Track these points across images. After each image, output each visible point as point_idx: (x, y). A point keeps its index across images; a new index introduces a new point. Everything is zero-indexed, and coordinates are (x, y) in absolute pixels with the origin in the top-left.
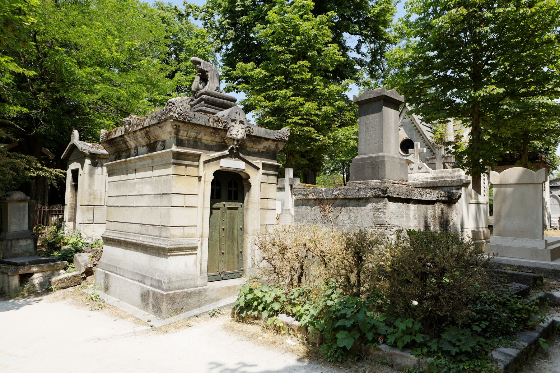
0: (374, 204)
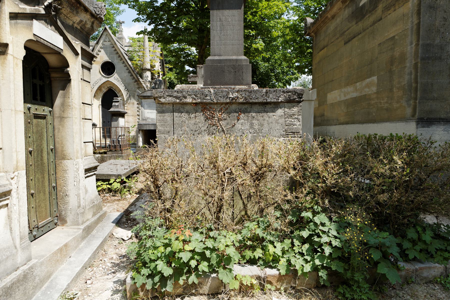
0: (286, 110)
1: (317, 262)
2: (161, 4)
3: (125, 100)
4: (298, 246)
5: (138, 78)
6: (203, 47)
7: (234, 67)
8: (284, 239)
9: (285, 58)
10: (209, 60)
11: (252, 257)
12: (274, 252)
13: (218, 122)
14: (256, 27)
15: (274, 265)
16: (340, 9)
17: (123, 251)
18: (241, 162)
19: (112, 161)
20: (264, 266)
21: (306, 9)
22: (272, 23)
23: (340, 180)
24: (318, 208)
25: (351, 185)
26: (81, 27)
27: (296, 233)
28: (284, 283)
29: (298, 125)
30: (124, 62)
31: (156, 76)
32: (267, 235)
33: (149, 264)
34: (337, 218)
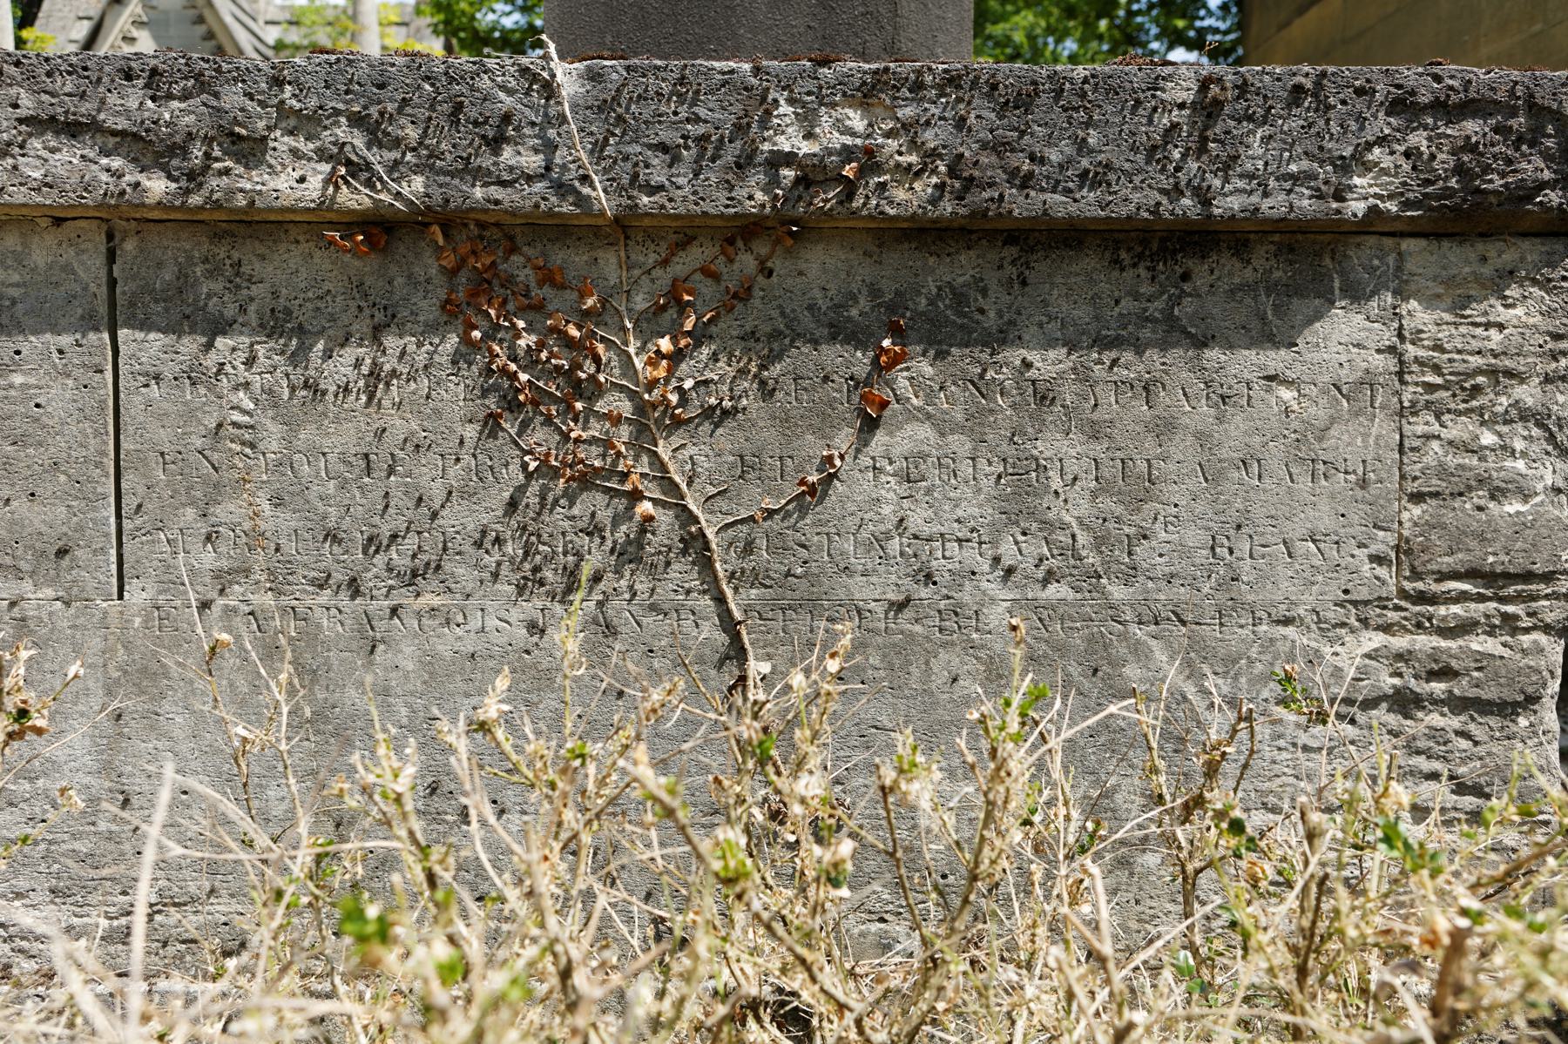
0: (1418, 315)
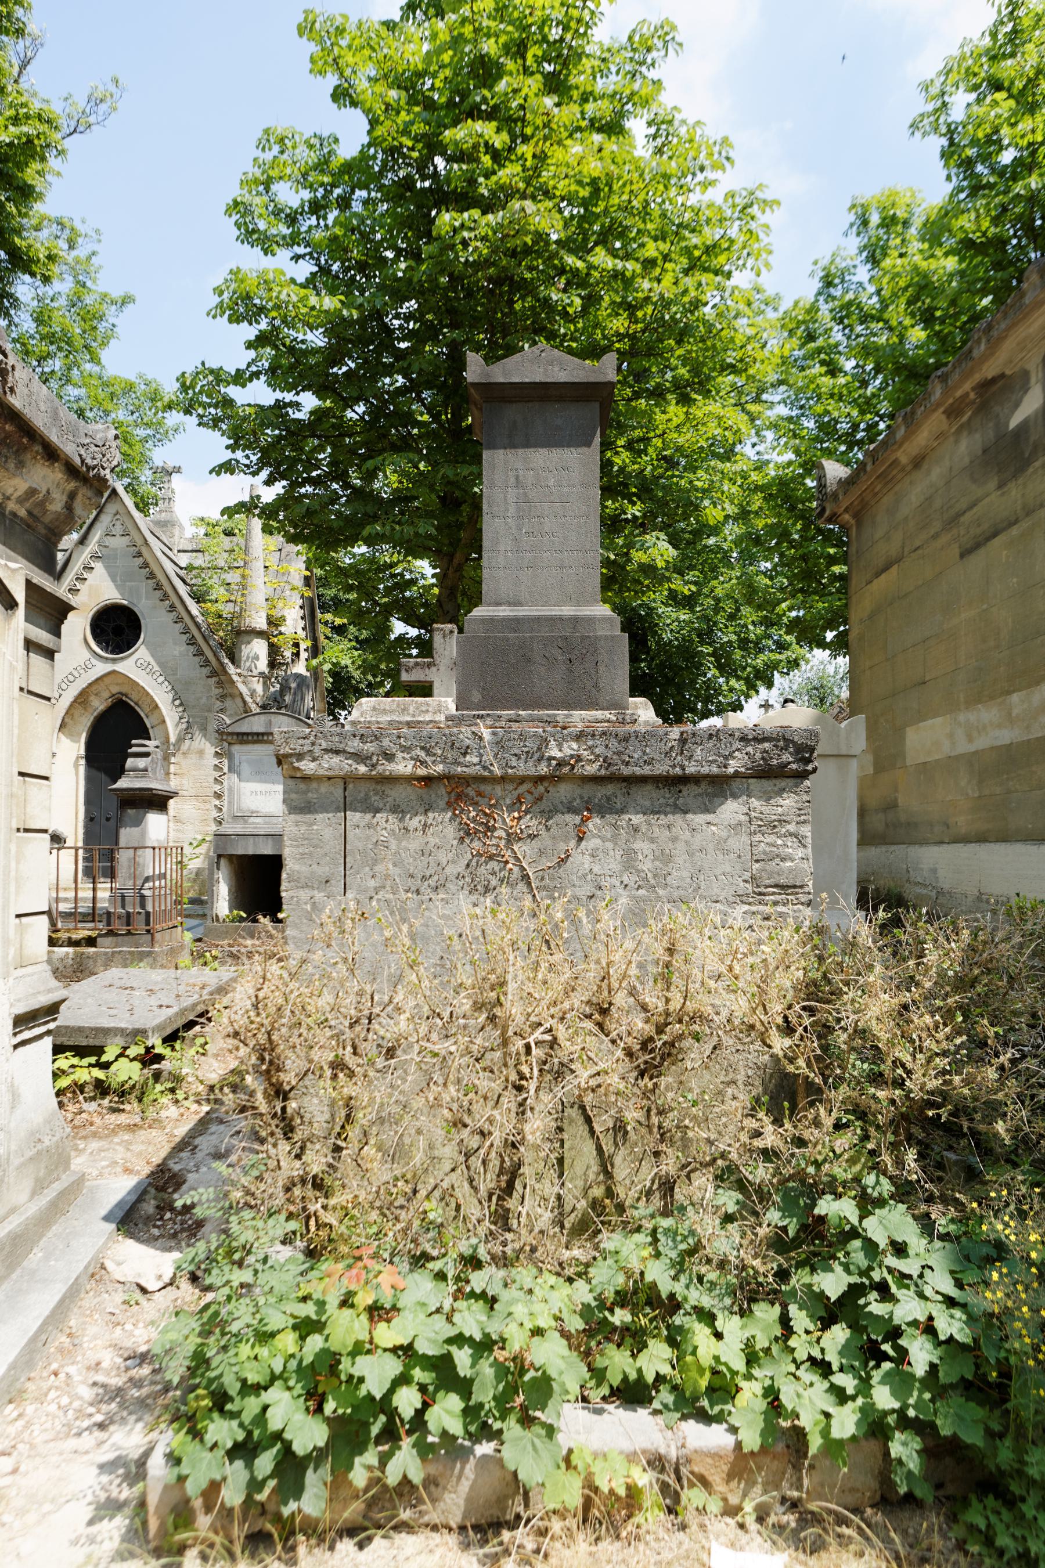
0: (755, 803)
1: (884, 1398)
2: (311, 413)
3: (173, 739)
4: (807, 1332)
5: (222, 664)
6: (458, 557)
7: (566, 644)
8: (752, 1300)
9: (750, 592)
10: (475, 619)
11: (633, 1376)
12: (717, 1358)
13: (507, 847)
14: (646, 489)
15: (717, 1409)
16: (941, 436)
17: (142, 1337)
18: (589, 1002)
19: (115, 973)
20: (676, 1410)
21: (821, 427)
22: (701, 479)
23: (957, 1079)
24: (878, 1183)
25: (1000, 1096)
26: (30, 513)
27: (800, 1278)
28: (755, 1483)
29: (798, 859)
30: (172, 608)
31: (288, 654)
32: (687, 1287)
33: (237, 1399)
34: (952, 1221)
